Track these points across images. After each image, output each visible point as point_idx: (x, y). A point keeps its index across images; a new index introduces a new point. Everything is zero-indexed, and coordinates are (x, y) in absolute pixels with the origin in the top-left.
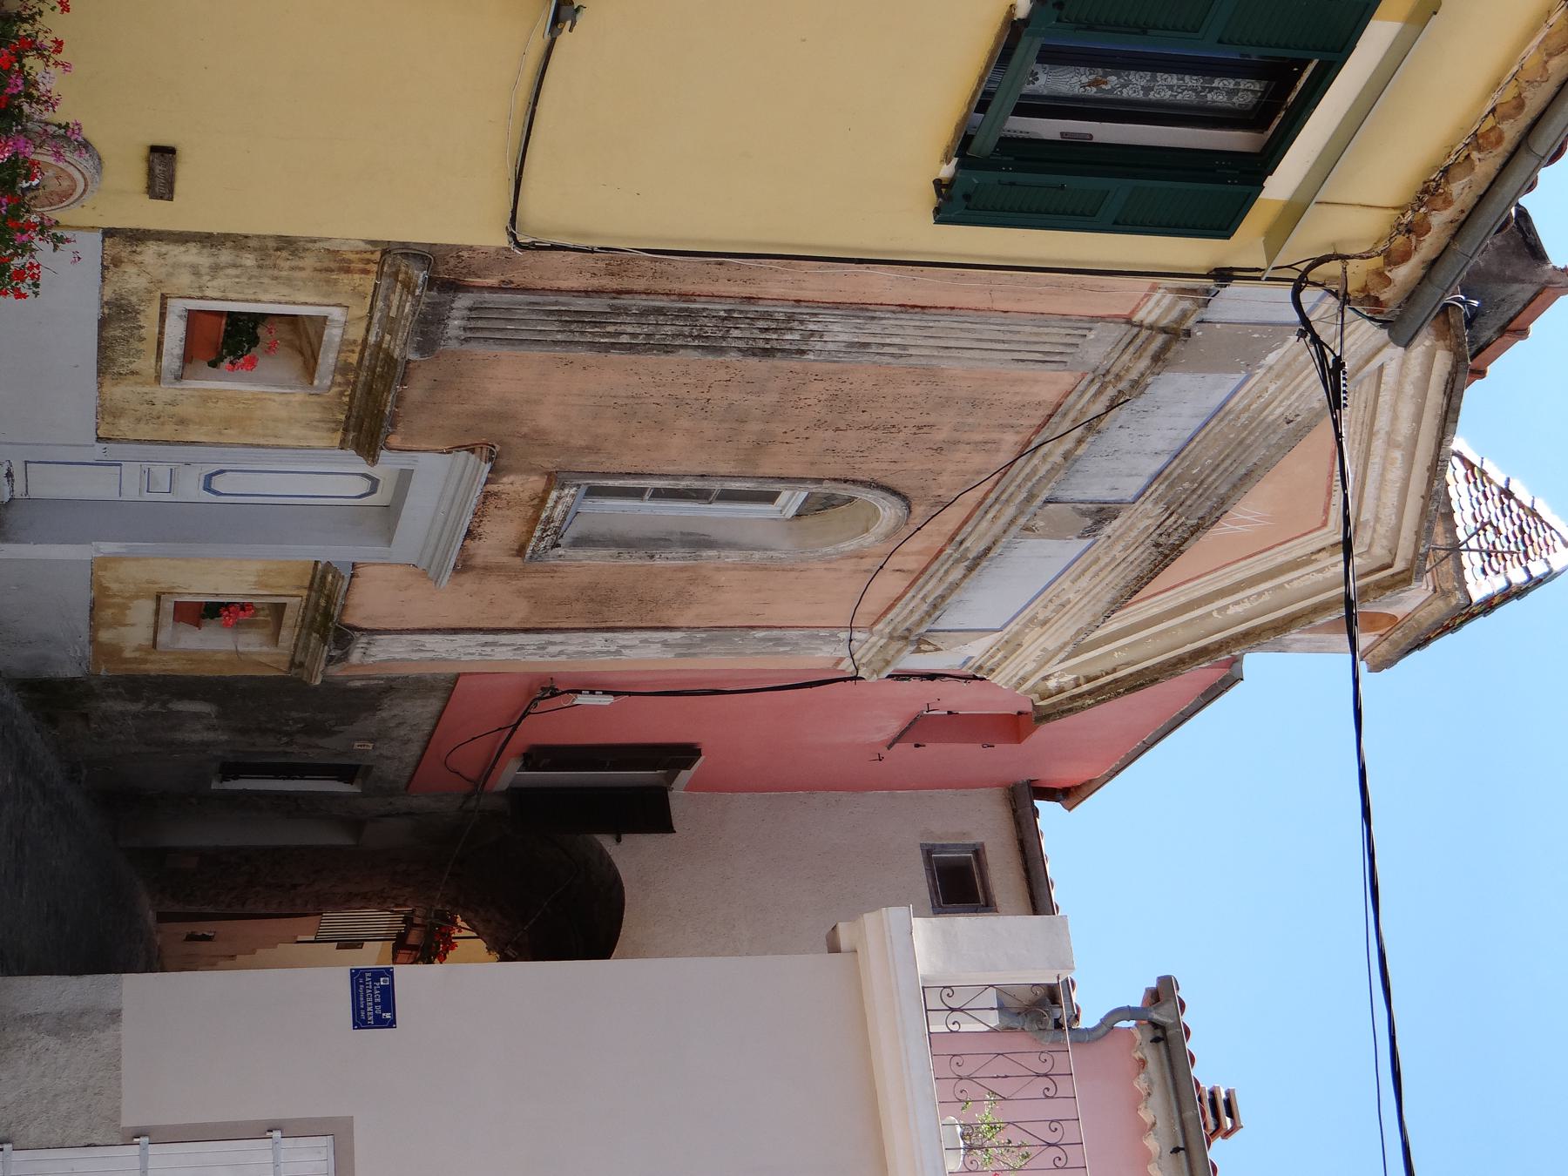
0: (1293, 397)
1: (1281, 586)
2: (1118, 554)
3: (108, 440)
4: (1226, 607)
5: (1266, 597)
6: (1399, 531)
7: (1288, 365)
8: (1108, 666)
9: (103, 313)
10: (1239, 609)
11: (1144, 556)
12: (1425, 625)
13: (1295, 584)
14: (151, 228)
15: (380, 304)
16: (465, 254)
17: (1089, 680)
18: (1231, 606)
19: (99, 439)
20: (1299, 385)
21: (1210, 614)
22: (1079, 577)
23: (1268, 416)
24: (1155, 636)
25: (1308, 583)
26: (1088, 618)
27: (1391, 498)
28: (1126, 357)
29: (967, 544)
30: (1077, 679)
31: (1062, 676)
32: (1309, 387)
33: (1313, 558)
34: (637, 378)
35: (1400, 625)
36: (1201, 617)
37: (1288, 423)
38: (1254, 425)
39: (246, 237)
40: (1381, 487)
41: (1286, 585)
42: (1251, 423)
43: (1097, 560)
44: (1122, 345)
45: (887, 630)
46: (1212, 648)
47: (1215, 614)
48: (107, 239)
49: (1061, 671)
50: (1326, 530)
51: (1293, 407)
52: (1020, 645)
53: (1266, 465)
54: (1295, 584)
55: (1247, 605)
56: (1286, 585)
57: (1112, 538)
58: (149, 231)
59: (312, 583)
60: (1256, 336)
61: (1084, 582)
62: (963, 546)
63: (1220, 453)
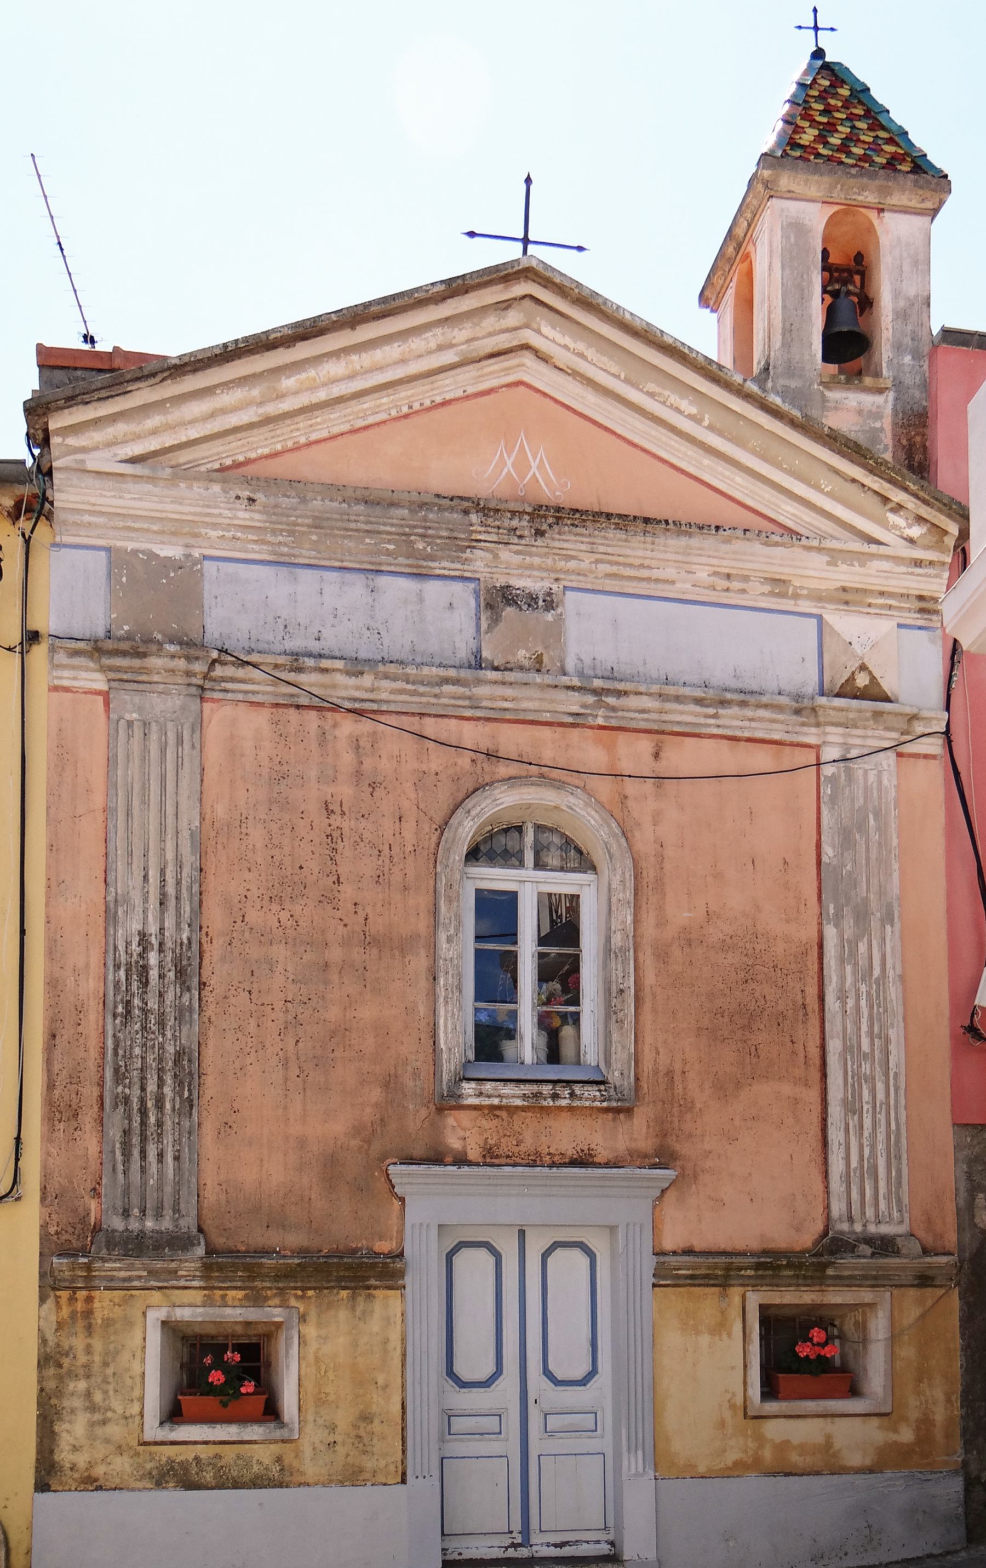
0: (216, 511)
1: (627, 381)
2: (587, 561)
3: (404, 1474)
4: (690, 417)
5: (651, 387)
6: (447, 319)
7: (173, 534)
8: (853, 492)
9: (175, 1487)
10: (684, 405)
11: (573, 538)
12: (826, 179)
13: (614, 369)
14: (34, 1458)
15: (136, 1283)
16: (52, 1230)
17: (886, 500)
18: (686, 413)
19: (404, 1481)
20: (200, 514)
21: (711, 428)
22: (666, 581)
23: (260, 521)
24: (778, 465)
25: (605, 359)
26: (739, 545)
27: (416, 344)
28: (156, 678)
29: (575, 709)
30: (892, 510)
31: (896, 527)
32: (190, 505)
33: (569, 371)
34: (780, 1002)
35: (849, 202)
36: (720, 433)
37: (254, 501)
38: (284, 527)
39: (42, 1390)
40: (380, 368)
41: (622, 377)
42: (282, 530)
43: (608, 576)
44: (141, 687)
45: (813, 730)
46: (756, 404)
47: (706, 423)
48: (52, 1489)
49: (890, 531)
50: (526, 379)
51: (231, 506)
52: (844, 589)
53: (333, 489)
54: (614, 369)
55: (674, 399)
56: (622, 377)
57: (556, 576)
58: (37, 1460)
59: (719, 1286)
60: (124, 579)
61: (670, 572)
62: (583, 711)
63: (345, 537)
